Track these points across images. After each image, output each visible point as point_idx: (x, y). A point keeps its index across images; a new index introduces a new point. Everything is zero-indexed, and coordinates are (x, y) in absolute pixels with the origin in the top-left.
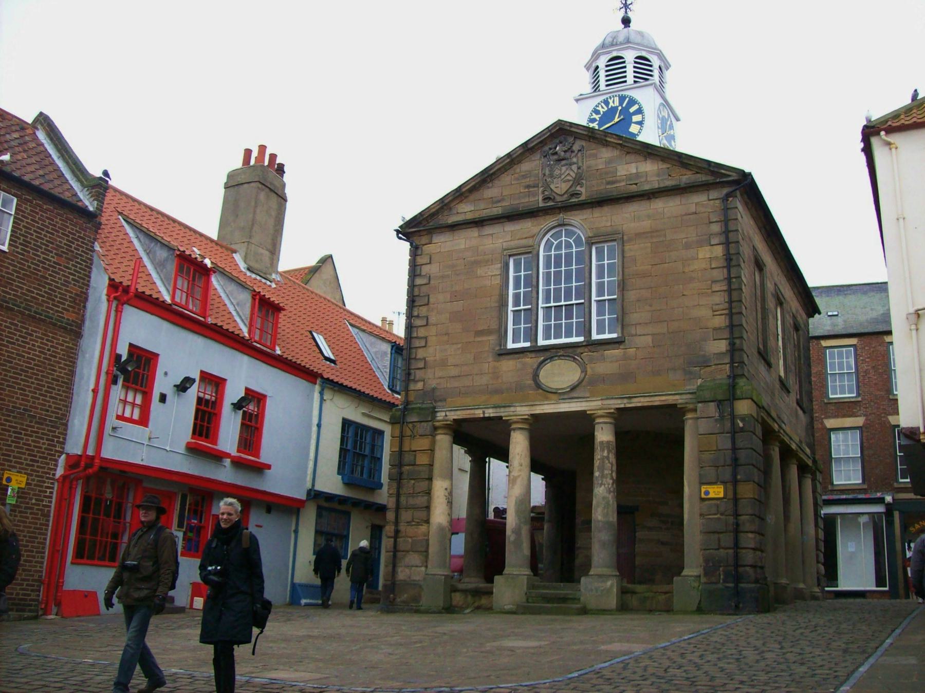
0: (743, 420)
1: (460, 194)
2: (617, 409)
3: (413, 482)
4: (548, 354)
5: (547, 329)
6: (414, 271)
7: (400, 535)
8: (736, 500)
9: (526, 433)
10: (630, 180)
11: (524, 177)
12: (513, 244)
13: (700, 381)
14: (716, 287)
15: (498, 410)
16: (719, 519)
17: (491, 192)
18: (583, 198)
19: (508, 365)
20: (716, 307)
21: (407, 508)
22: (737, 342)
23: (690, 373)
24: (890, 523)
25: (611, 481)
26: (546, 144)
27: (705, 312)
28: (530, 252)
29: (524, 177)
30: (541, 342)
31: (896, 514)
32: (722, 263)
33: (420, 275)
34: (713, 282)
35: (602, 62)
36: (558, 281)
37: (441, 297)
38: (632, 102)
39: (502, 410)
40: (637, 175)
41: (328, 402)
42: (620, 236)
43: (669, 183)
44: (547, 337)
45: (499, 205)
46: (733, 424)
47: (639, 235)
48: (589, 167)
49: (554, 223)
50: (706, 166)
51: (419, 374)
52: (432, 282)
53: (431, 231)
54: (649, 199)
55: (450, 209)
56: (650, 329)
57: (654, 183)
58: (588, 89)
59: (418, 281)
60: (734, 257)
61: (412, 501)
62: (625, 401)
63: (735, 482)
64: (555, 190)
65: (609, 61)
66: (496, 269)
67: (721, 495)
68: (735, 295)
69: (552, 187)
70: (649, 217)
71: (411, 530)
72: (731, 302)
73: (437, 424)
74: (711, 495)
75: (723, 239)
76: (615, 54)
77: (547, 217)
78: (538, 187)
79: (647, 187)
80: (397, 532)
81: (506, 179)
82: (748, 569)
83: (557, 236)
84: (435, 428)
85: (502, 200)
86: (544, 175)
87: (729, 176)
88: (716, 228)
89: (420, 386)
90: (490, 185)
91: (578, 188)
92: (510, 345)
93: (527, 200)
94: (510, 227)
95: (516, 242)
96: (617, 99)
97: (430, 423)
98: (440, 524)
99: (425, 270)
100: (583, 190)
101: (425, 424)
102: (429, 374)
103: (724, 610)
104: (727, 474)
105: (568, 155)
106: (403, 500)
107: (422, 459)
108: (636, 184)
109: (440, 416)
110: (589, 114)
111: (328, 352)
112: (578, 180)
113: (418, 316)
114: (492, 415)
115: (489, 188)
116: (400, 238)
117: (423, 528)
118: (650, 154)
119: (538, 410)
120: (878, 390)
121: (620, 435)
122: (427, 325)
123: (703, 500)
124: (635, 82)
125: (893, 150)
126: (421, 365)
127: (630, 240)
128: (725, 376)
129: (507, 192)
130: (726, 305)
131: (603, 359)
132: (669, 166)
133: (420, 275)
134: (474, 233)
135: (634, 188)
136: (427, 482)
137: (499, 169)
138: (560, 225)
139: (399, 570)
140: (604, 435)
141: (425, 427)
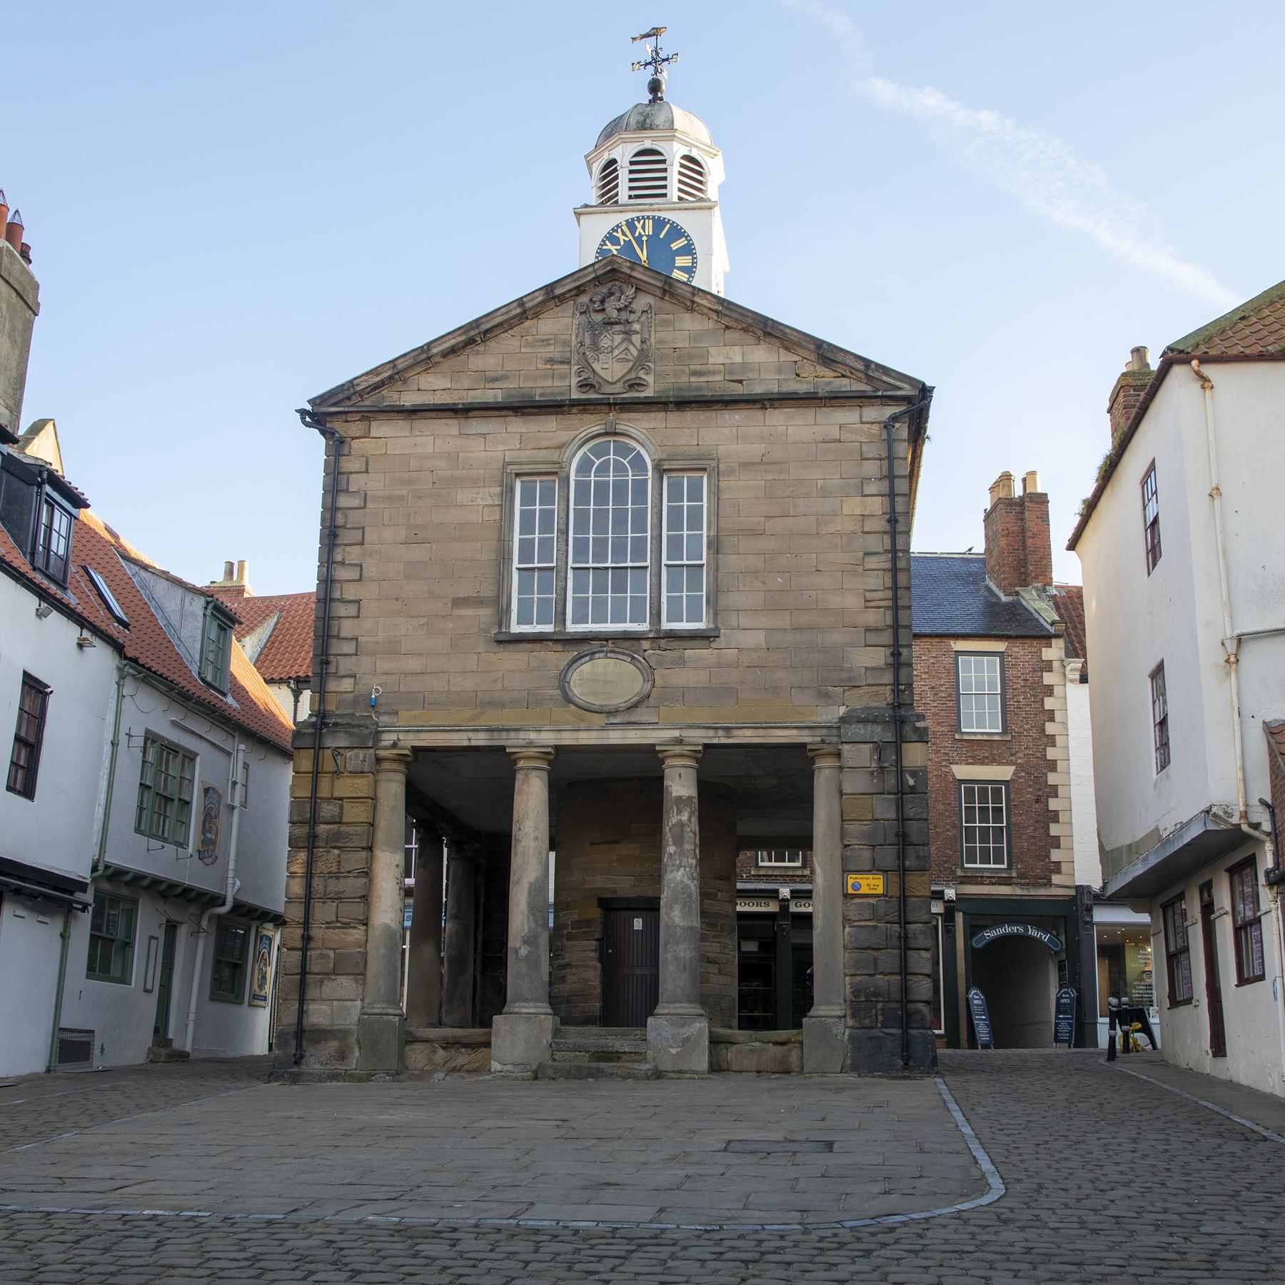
0: (914, 774)
1: (424, 358)
2: (706, 746)
3: (337, 852)
4: (586, 648)
5: (581, 604)
6: (335, 483)
7: (312, 945)
8: (903, 899)
9: (545, 775)
10: (731, 373)
11: (546, 342)
12: (526, 455)
13: (842, 710)
14: (872, 563)
15: (496, 735)
16: (875, 927)
17: (485, 360)
18: (649, 393)
19: (515, 659)
20: (869, 595)
21: (326, 898)
22: (904, 651)
23: (826, 695)
24: (950, 932)
25: (694, 862)
26: (584, 292)
27: (852, 602)
28: (556, 473)
29: (546, 342)
30: (572, 628)
31: (959, 917)
32: (882, 525)
33: (347, 491)
34: (866, 554)
35: (623, 152)
36: (601, 527)
37: (388, 534)
38: (677, 232)
39: (504, 735)
40: (744, 366)
41: (128, 698)
42: (714, 463)
43: (802, 388)
44: (580, 619)
45: (497, 385)
46: (900, 779)
47: (746, 465)
48: (661, 342)
49: (598, 429)
50: (860, 366)
51: (345, 665)
52: (369, 505)
53: (369, 415)
54: (764, 408)
55: (405, 381)
56: (765, 621)
57: (767, 383)
58: (593, 198)
59: (344, 501)
60: (900, 519)
61: (334, 886)
62: (711, 733)
63: (903, 871)
64: (602, 373)
65: (637, 155)
66: (488, 495)
67: (880, 891)
68: (902, 578)
69: (597, 367)
70: (762, 438)
71: (334, 936)
72: (895, 588)
73: (383, 753)
74: (864, 890)
75: (884, 487)
76: (648, 144)
77: (586, 417)
78: (569, 363)
79: (759, 389)
80: (307, 939)
81: (509, 342)
82: (921, 1006)
83: (600, 452)
84: (379, 760)
85: (505, 377)
86: (582, 344)
87: (900, 389)
88: (872, 468)
89: (347, 685)
90: (481, 348)
91: (642, 374)
92: (516, 628)
93: (549, 383)
94: (517, 426)
95: (528, 453)
96: (649, 224)
97: (371, 751)
98: (387, 926)
99: (357, 482)
100: (650, 379)
101: (361, 753)
102: (362, 665)
103: (888, 1071)
104: (888, 856)
105: (624, 316)
106: (317, 883)
107: (355, 813)
108: (740, 382)
109: (388, 739)
110: (599, 241)
111: (118, 611)
112: (642, 360)
113: (343, 563)
114: (482, 743)
115: (478, 353)
116: (308, 425)
117: (357, 934)
118: (767, 334)
119: (568, 739)
120: (939, 724)
121: (703, 786)
122: (360, 580)
123: (847, 896)
124: (680, 198)
125: (1207, 391)
126: (349, 648)
127: (731, 472)
128: (883, 704)
129: (520, 365)
130: (889, 594)
131: (682, 662)
132: (796, 358)
133: (347, 491)
134: (451, 427)
135: (739, 390)
136: (364, 854)
137: (500, 325)
138: (606, 434)
139: (312, 1007)
140: (681, 785)
141: (356, 758)
